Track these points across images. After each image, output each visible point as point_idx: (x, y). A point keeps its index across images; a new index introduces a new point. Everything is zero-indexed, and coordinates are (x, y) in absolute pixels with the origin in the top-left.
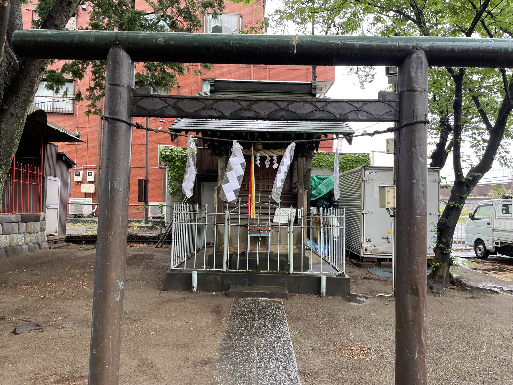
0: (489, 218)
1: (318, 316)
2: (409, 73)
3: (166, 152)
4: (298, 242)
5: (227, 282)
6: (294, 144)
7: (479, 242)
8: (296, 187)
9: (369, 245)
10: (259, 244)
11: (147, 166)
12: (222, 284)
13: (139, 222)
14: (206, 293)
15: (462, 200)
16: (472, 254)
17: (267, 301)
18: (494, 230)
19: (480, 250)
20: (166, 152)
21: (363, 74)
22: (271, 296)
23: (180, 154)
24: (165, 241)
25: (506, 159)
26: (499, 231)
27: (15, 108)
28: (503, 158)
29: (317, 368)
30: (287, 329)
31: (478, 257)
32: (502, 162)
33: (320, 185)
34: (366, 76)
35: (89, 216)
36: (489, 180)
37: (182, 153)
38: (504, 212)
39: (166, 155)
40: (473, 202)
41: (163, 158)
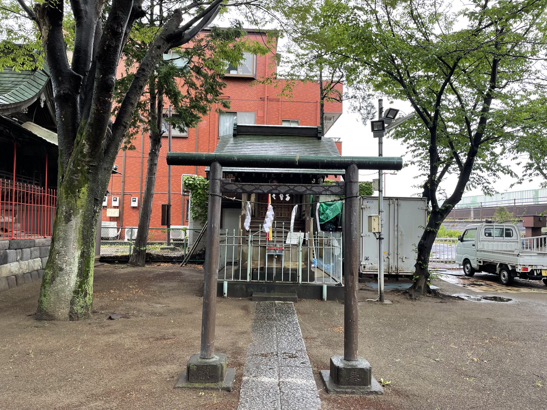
0: (474, 240)
1: (319, 312)
2: (349, 174)
3: (189, 181)
4: (306, 259)
5: (250, 290)
6: (297, 205)
7: (466, 261)
8: (304, 215)
9: (367, 263)
10: (275, 260)
11: (169, 192)
12: (247, 291)
13: (162, 244)
14: (234, 298)
15: (437, 226)
16: (462, 272)
17: (281, 303)
18: (478, 250)
19: (468, 268)
20: (189, 181)
21: (366, 112)
22: (285, 299)
23: (202, 183)
24: (188, 261)
25: (488, 189)
26: (481, 251)
27: (107, 164)
28: (486, 187)
29: (316, 336)
30: (296, 318)
31: (466, 275)
32: (486, 191)
33: (328, 211)
34: (369, 114)
35: (114, 238)
36: (507, 202)
37: (203, 182)
38: (487, 235)
39: (189, 184)
40: (465, 224)
41: (187, 186)
